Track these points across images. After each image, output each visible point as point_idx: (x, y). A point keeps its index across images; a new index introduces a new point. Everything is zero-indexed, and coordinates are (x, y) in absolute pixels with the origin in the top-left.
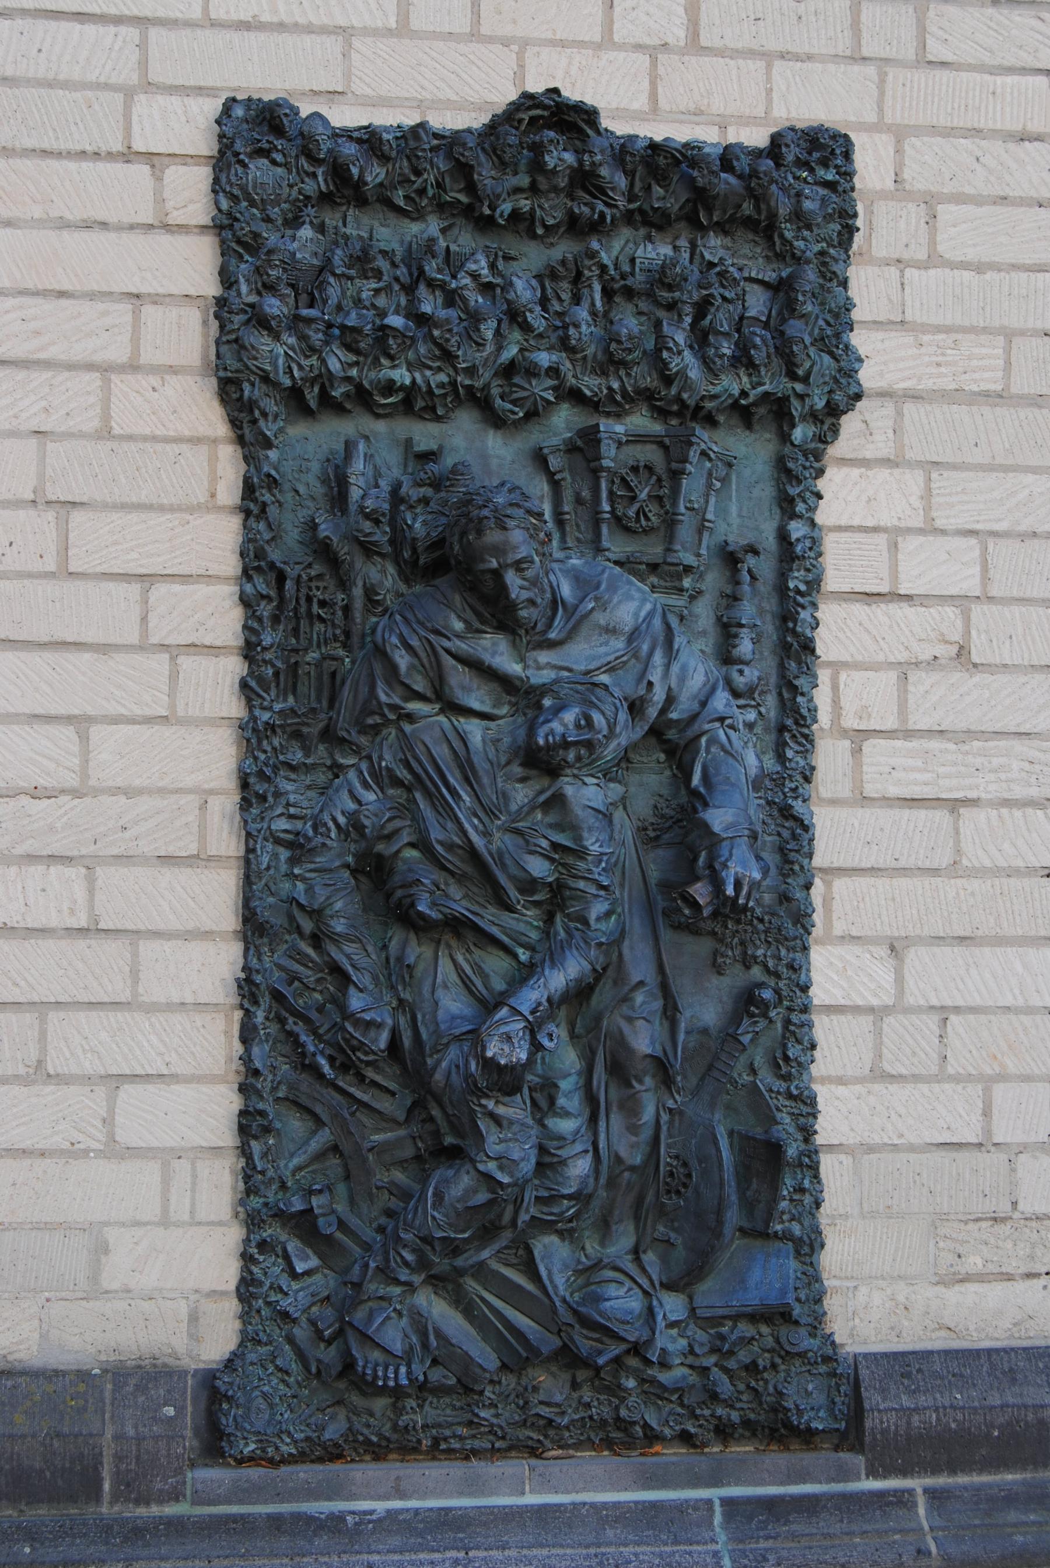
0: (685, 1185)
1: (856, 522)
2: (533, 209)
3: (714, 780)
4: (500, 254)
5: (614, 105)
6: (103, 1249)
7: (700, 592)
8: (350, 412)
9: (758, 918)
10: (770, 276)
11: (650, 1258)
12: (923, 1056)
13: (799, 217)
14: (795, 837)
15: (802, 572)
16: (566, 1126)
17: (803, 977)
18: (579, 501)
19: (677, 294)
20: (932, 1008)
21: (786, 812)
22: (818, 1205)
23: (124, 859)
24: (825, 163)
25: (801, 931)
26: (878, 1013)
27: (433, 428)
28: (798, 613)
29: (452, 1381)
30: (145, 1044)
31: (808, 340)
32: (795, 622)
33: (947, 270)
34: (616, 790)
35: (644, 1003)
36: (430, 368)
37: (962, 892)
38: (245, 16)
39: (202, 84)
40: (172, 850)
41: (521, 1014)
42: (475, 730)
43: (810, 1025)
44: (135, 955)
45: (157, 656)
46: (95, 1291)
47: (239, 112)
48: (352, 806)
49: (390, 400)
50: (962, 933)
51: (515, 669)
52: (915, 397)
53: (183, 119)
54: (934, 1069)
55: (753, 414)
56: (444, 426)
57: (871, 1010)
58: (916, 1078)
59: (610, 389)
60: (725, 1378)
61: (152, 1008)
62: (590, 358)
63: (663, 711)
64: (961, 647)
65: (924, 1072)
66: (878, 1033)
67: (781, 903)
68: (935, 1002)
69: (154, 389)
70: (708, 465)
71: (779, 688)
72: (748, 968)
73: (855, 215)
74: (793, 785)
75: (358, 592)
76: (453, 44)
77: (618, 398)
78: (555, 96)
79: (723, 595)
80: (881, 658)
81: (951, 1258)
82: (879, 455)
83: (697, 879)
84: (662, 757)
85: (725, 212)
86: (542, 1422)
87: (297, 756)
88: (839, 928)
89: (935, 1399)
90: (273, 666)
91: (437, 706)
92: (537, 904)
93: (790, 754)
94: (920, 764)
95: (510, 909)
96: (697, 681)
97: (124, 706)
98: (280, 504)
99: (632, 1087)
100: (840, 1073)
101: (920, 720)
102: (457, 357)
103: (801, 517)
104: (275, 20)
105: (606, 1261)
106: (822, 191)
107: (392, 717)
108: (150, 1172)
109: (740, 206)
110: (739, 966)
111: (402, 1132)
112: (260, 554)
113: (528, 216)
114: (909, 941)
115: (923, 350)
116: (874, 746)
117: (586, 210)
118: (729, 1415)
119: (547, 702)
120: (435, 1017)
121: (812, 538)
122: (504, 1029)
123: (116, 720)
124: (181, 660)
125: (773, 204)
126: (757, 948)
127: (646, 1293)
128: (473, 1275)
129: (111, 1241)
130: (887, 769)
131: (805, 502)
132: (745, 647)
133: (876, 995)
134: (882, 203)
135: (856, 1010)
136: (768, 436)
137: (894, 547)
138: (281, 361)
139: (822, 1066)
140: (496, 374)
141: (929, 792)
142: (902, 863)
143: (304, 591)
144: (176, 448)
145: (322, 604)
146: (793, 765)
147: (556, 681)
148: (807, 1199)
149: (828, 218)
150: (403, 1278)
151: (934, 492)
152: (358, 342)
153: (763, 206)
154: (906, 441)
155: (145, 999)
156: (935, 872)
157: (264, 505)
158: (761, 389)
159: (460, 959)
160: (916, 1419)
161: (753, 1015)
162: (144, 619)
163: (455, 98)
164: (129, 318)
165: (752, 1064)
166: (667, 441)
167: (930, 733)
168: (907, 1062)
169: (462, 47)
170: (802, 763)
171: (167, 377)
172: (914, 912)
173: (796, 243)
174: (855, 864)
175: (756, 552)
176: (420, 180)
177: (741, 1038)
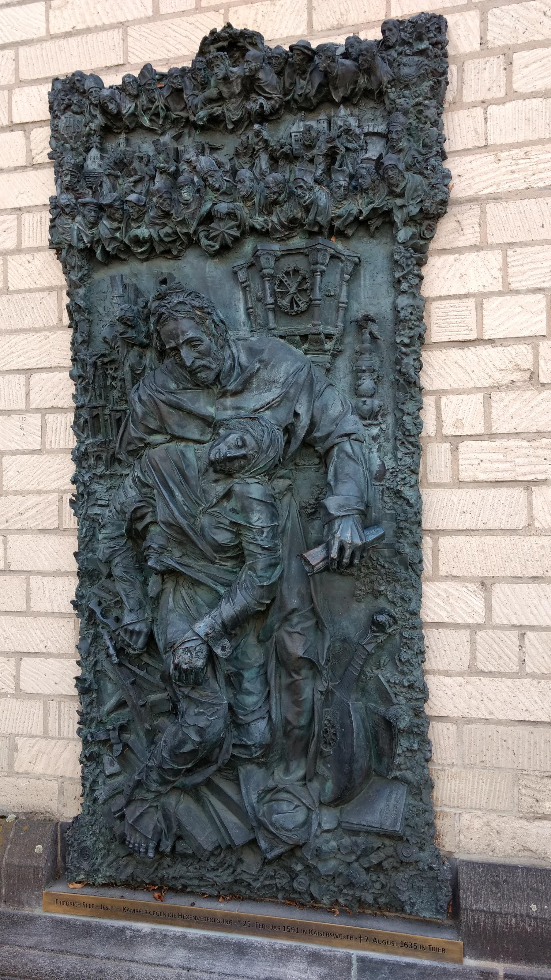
1: (452, 293)
2: (223, 112)
4: (206, 146)
6: (15, 749)
7: (341, 352)
8: (125, 260)
15: (407, 331)
16: (250, 700)
20: (513, 626)
23: (21, 531)
24: (420, 38)
31: (401, 166)
36: (157, 224)
37: (535, 546)
38: (68, 28)
40: (44, 525)
43: (422, 638)
44: (28, 584)
45: (35, 415)
46: (11, 773)
49: (143, 249)
50: (535, 574)
51: (211, 410)
52: (495, 198)
54: (516, 669)
56: (179, 262)
57: (467, 626)
58: (502, 674)
61: (37, 615)
62: (257, 204)
63: (310, 431)
64: (532, 373)
65: (508, 670)
66: (473, 642)
68: (515, 622)
69: (29, 262)
70: (342, 265)
71: (394, 411)
72: (376, 598)
74: (402, 476)
75: (127, 368)
76: (185, 18)
77: (279, 228)
78: (228, 30)
80: (471, 385)
81: (530, 801)
82: (469, 243)
84: (317, 461)
85: (346, 88)
87: (100, 470)
88: (443, 571)
89: (515, 907)
92: (232, 558)
93: (400, 455)
99: (292, 677)
100: (447, 668)
101: (500, 427)
103: (404, 292)
104: (84, 27)
106: (416, 58)
108: (37, 707)
109: (356, 82)
110: (370, 596)
114: (495, 580)
115: (501, 163)
116: (467, 446)
119: (222, 431)
122: (187, 645)
123: (15, 453)
124: (47, 416)
126: (380, 585)
129: (20, 745)
130: (477, 462)
134: (470, 62)
135: (457, 626)
136: (384, 240)
137: (480, 307)
139: (434, 663)
144: (41, 294)
146: (403, 463)
149: (422, 78)
151: (510, 265)
155: (35, 609)
156: (513, 532)
158: (371, 206)
160: (499, 921)
162: (28, 395)
164: (15, 223)
167: (508, 435)
168: (495, 663)
169: (191, 19)
171: (35, 254)
173: (398, 101)
174: (455, 527)
175: (373, 321)
176: (154, 107)
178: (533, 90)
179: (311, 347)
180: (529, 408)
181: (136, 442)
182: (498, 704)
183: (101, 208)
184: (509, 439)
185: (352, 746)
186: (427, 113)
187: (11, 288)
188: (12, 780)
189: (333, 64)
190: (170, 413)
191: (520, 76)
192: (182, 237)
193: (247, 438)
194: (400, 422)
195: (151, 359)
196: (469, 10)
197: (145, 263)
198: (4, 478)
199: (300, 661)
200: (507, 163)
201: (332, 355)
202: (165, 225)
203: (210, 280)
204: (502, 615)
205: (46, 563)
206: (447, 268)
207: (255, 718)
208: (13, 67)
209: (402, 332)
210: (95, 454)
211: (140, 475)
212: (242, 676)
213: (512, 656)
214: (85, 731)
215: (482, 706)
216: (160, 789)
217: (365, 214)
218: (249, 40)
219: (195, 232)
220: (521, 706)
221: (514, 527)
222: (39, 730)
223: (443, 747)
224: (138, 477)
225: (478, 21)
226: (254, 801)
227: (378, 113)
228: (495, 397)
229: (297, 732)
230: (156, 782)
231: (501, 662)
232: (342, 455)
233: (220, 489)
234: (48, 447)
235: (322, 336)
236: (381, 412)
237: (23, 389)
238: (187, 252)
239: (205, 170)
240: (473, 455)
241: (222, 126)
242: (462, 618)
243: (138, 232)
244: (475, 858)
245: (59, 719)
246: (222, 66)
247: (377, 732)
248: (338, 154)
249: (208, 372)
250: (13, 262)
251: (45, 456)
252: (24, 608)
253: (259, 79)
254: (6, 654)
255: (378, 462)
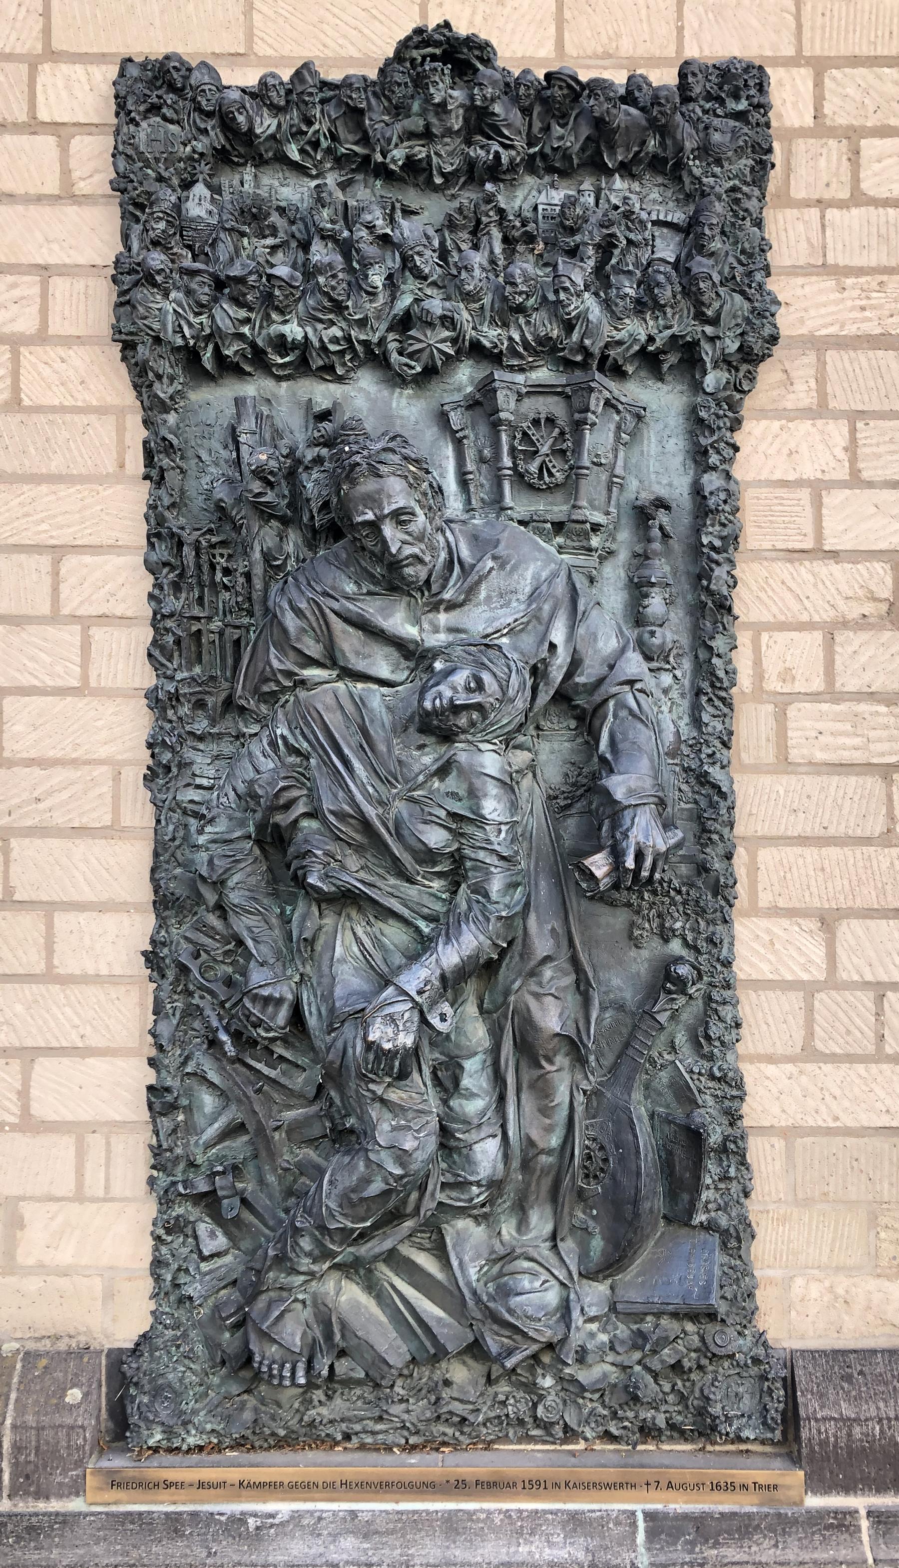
0: (602, 1170)
2: (429, 157)
3: (621, 746)
4: (398, 205)
5: (519, 55)
6: (17, 1223)
7: (611, 553)
8: (250, 374)
9: (675, 889)
10: (678, 216)
11: (568, 1246)
12: (859, 1035)
13: (705, 151)
14: (713, 805)
15: (717, 528)
17: (725, 952)
18: (482, 460)
19: (578, 238)
21: (703, 779)
22: (747, 1195)
24: (737, 97)
25: (723, 903)
26: (809, 989)
27: (335, 389)
28: (712, 570)
29: (362, 1375)
30: (60, 1016)
31: (716, 278)
32: (709, 580)
33: (872, 209)
34: (521, 758)
35: (552, 978)
36: (321, 321)
39: (105, 51)
41: (408, 994)
42: (376, 697)
44: (50, 926)
47: (133, 71)
48: (252, 774)
49: (287, 359)
51: (411, 631)
53: (87, 87)
55: (661, 362)
58: (850, 1059)
59: (510, 339)
60: (649, 1379)
62: (488, 307)
63: (569, 675)
66: (810, 1010)
67: (699, 874)
68: (869, 977)
70: (617, 418)
71: (694, 649)
73: (770, 150)
74: (710, 751)
75: (257, 555)
78: (445, 31)
79: (636, 555)
80: (805, 617)
83: (598, 849)
84: (573, 724)
85: (628, 150)
86: (456, 1419)
87: (201, 725)
88: (765, 899)
89: (878, 1408)
90: (174, 634)
91: (335, 673)
92: (440, 875)
93: (705, 718)
94: (848, 727)
95: (411, 881)
96: (608, 644)
97: (36, 677)
98: (183, 472)
99: (542, 1067)
100: (770, 1051)
102: (347, 307)
103: (714, 468)
105: (518, 1251)
106: (732, 123)
107: (288, 683)
109: (643, 143)
111: (314, 1109)
112: (161, 521)
113: (424, 164)
117: (482, 153)
118: (654, 1418)
119: (438, 665)
120: (332, 993)
121: (727, 490)
122: (389, 1010)
125: (679, 137)
126: (676, 921)
127: (562, 1284)
128: (384, 1261)
130: (814, 734)
131: (718, 453)
132: (656, 604)
133: (807, 970)
134: (801, 141)
136: (679, 387)
137: (818, 504)
138: (170, 318)
139: (750, 1044)
140: (390, 329)
141: (859, 757)
142: (832, 831)
143: (204, 557)
144: (85, 419)
145: (227, 572)
146: (710, 729)
147: (449, 645)
148: (735, 1187)
149: (740, 152)
150: (303, 1269)
151: (860, 442)
152: (245, 295)
153: (669, 142)
154: (829, 390)
155: (61, 971)
156: (867, 841)
157: (162, 470)
158: (668, 333)
159: (360, 931)
160: (857, 1431)
161: (670, 992)
163: (356, 55)
164: (36, 290)
165: (672, 1042)
166: (568, 390)
168: (841, 1041)
170: (720, 727)
172: (846, 882)
173: (705, 180)
175: (667, 508)
176: (311, 130)
177: (658, 1017)
178: (888, 195)
179: (569, 542)
180: (888, 656)
181: (280, 677)
182: (846, 1103)
183: (219, 284)
184: (859, 701)
185: (639, 1174)
186: (747, 204)
187: (26, 402)
188: (11, 1280)
189: (615, 111)
190: (344, 632)
191: (869, 172)
192: (358, 347)
193: (486, 677)
194: (705, 667)
195: (296, 545)
196: (799, 65)
197: (284, 384)
198: (5, 736)
199: (556, 1040)
200: (856, 293)
201: (600, 557)
202: (332, 323)
203: (398, 422)
204: (850, 967)
205: (86, 889)
206: (770, 439)
207: (483, 1135)
208: (40, 26)
209: (710, 529)
210: (193, 699)
211: (286, 732)
212: (462, 1068)
213: (866, 1029)
214: (163, 1180)
215: (823, 1109)
216: (315, 1268)
217: (659, 343)
218: (477, 53)
219: (382, 341)
220: (879, 1106)
221: (868, 834)
222: (67, 1187)
223: (764, 1175)
224: (283, 737)
225: (810, 85)
226: (474, 1278)
227: (669, 193)
228: (839, 638)
229: (544, 1159)
230: (308, 1254)
231: (849, 1039)
232: (623, 713)
233: (428, 759)
234: (93, 683)
235: (588, 526)
236: (674, 652)
237: (48, 580)
238: (360, 373)
239: (411, 243)
240: (808, 724)
241: (421, 179)
242: (793, 972)
243: (286, 329)
244: (812, 1344)
245: (108, 1165)
246: (441, 85)
247: (670, 1153)
248: (616, 246)
249: (419, 567)
250: (32, 358)
251: (88, 699)
252: (40, 967)
253: (494, 114)
254: (4, 1052)
255: (672, 728)
